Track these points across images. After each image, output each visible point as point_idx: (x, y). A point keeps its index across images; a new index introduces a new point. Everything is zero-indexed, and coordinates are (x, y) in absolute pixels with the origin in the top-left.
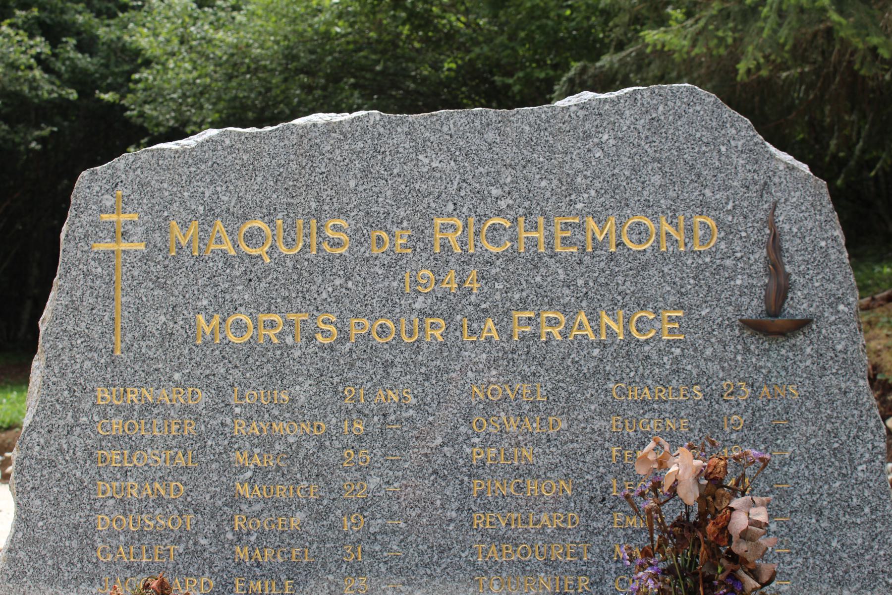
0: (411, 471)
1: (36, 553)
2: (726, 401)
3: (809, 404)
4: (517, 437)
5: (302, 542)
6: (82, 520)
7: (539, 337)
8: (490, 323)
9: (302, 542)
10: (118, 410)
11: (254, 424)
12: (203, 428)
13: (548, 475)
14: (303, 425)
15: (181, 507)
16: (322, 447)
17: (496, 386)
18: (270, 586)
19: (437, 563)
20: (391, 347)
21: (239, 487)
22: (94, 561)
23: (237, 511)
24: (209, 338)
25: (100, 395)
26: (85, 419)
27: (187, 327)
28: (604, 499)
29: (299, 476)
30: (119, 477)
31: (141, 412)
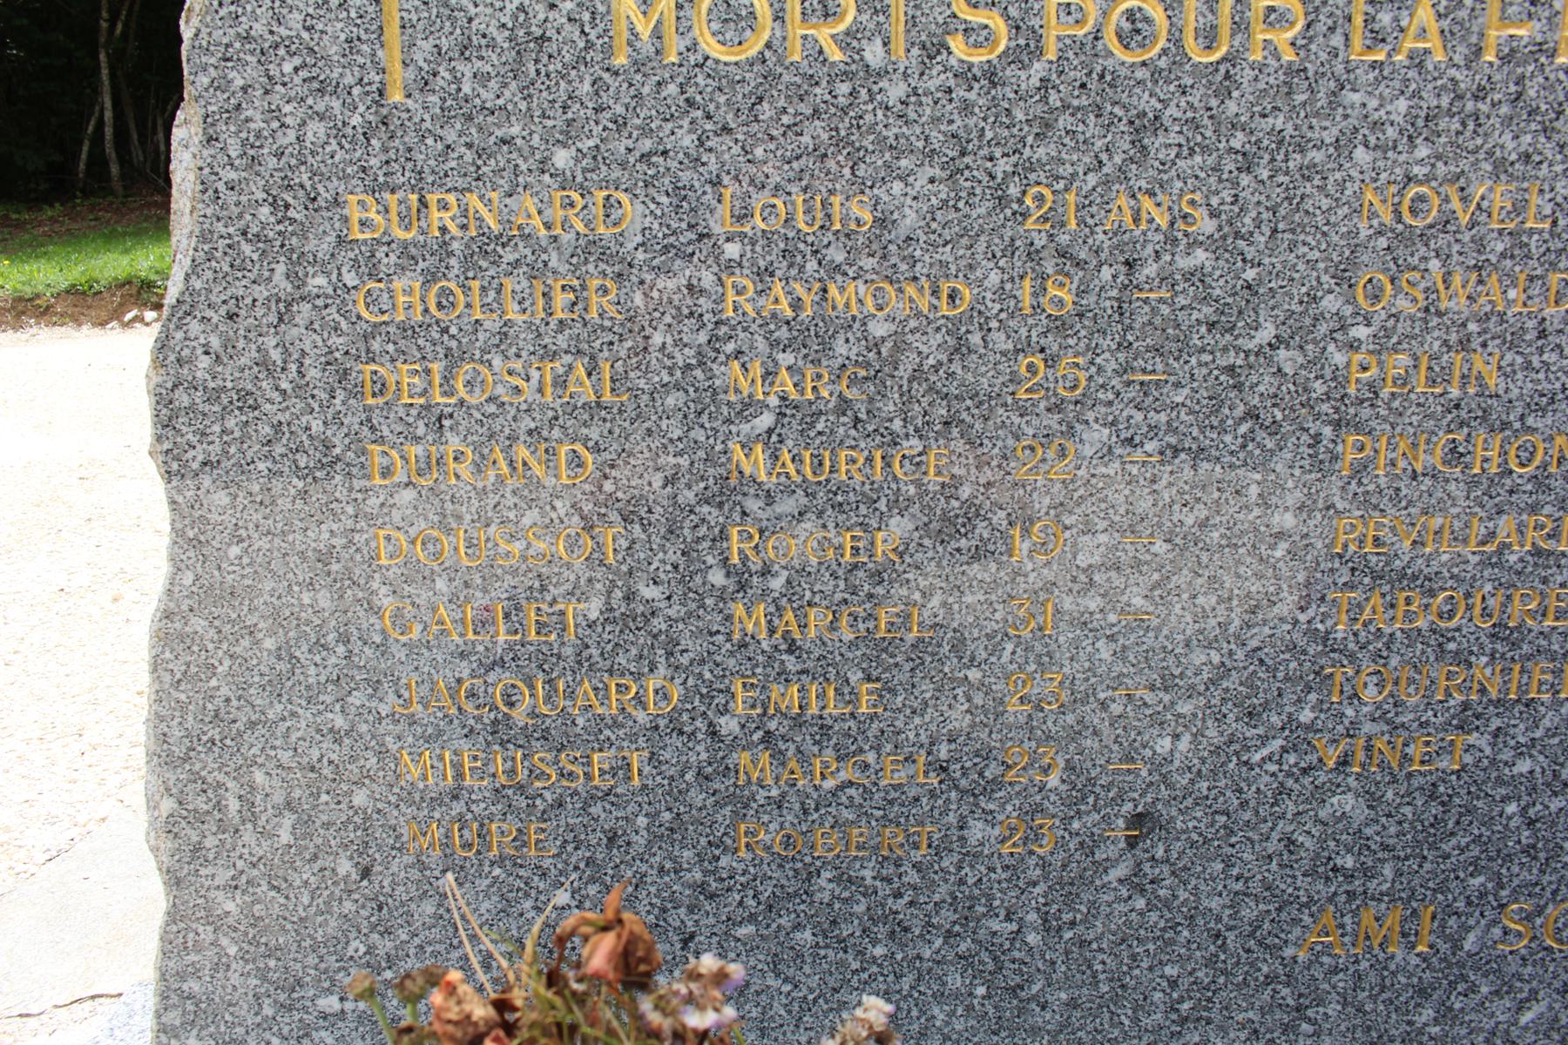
0: (1191, 412)
1: (232, 622)
4: (1464, 325)
5: (904, 592)
6: (339, 542)
9: (904, 592)
10: (409, 255)
11: (778, 288)
12: (638, 299)
13: (1530, 421)
14: (911, 290)
15: (587, 507)
16: (960, 349)
17: (1423, 189)
18: (822, 696)
19: (1237, 637)
20: (1156, 74)
21: (738, 453)
22: (378, 639)
23: (737, 517)
24: (646, 46)
25: (356, 215)
26: (321, 281)
27: (586, 16)
29: (897, 425)
30: (421, 431)
31: (467, 259)
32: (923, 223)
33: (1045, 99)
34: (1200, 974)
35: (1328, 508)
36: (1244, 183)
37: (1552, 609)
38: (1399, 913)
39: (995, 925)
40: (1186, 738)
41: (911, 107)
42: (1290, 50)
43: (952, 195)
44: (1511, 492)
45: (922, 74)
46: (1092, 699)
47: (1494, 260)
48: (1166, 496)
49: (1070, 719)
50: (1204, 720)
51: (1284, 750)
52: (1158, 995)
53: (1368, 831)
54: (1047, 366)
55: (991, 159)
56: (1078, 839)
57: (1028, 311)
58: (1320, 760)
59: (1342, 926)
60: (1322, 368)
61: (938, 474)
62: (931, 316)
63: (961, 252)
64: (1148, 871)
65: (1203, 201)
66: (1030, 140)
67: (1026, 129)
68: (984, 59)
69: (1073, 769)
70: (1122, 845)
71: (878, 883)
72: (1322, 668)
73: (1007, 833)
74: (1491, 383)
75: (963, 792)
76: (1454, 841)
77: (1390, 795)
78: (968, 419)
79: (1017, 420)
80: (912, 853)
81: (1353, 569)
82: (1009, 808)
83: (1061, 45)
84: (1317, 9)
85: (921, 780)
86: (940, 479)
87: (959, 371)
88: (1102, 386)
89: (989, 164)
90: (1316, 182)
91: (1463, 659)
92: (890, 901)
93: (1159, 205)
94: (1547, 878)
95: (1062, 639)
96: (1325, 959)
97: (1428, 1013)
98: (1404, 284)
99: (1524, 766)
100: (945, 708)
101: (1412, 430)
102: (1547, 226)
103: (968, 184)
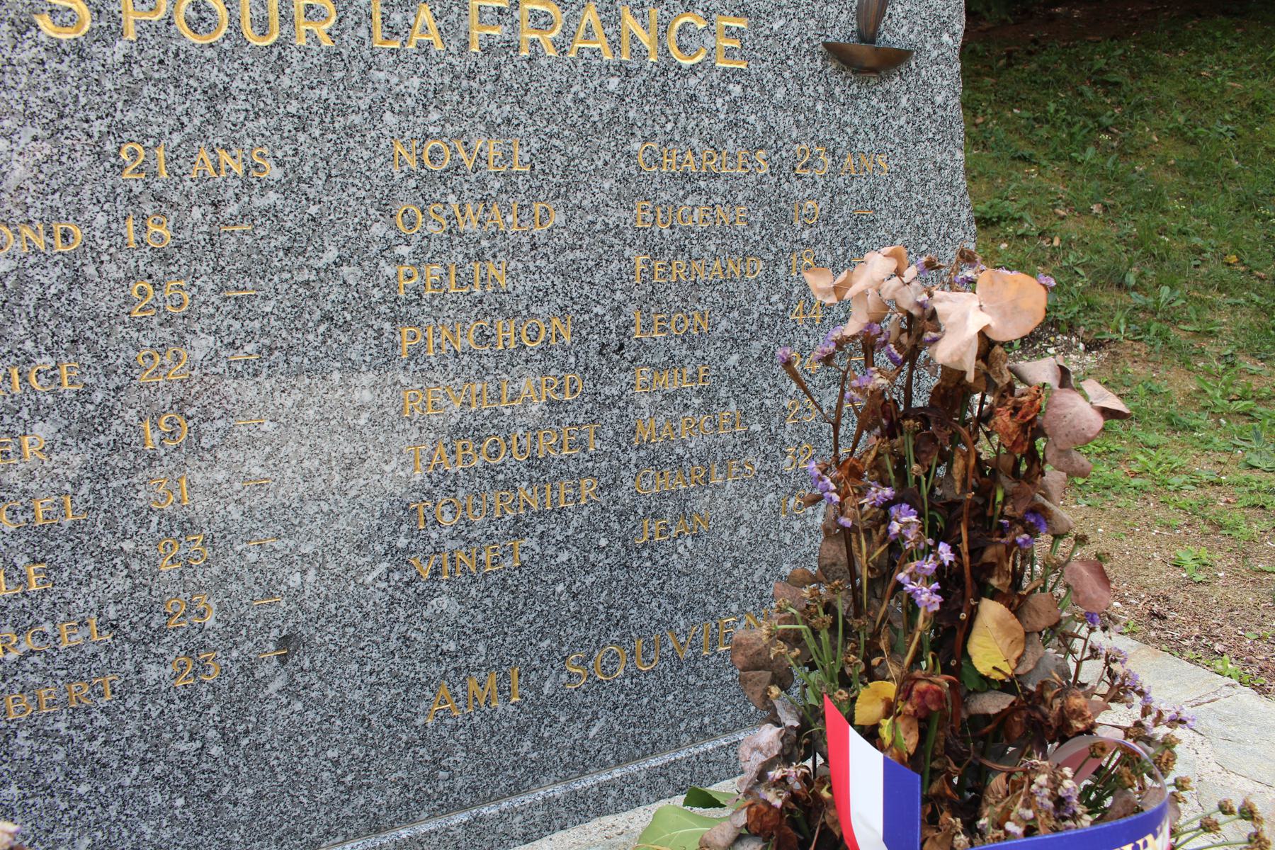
2: (799, 177)
3: (900, 185)
4: (478, 242)
7: (517, 50)
8: (425, 15)
13: (533, 309)
14: (27, 232)
16: (77, 279)
17: (438, 144)
20: (222, 54)
28: (621, 347)
29: (29, 345)
32: (31, 175)
33: (129, 72)
34: (355, 752)
35: (395, 384)
36: (301, 140)
37: (566, 443)
38: (494, 677)
39: (182, 747)
40: (312, 573)
41: (8, 75)
42: (328, 38)
43: (55, 151)
44: (527, 361)
45: (15, 47)
46: (231, 552)
47: (494, 195)
48: (267, 386)
49: (216, 570)
50: (323, 556)
51: (390, 571)
52: (326, 775)
53: (462, 621)
54: (155, 290)
55: (87, 121)
56: (239, 665)
57: (134, 245)
58: (418, 574)
59: (456, 694)
60: (377, 279)
61: (72, 383)
62: (48, 253)
63: (69, 199)
64: (300, 680)
65: (271, 154)
66: (120, 105)
67: (116, 96)
68: (72, 37)
69: (225, 609)
70: (276, 663)
71: (72, 732)
72: (408, 504)
73: (179, 670)
74: (503, 283)
75: (135, 643)
76: (524, 618)
77: (473, 592)
78: (92, 337)
79: (135, 335)
80: (99, 700)
81: (420, 428)
82: (177, 649)
83: (139, 28)
84: (345, 8)
85: (96, 638)
86: (75, 388)
87: (79, 298)
88: (204, 303)
89: (86, 125)
90: (357, 139)
91: (510, 486)
92: (86, 744)
93: (234, 157)
94: (591, 632)
95: (198, 507)
96: (448, 721)
97: (527, 744)
98: (432, 214)
99: (564, 556)
100: (107, 576)
101: (450, 321)
102: (528, 170)
103: (69, 142)
